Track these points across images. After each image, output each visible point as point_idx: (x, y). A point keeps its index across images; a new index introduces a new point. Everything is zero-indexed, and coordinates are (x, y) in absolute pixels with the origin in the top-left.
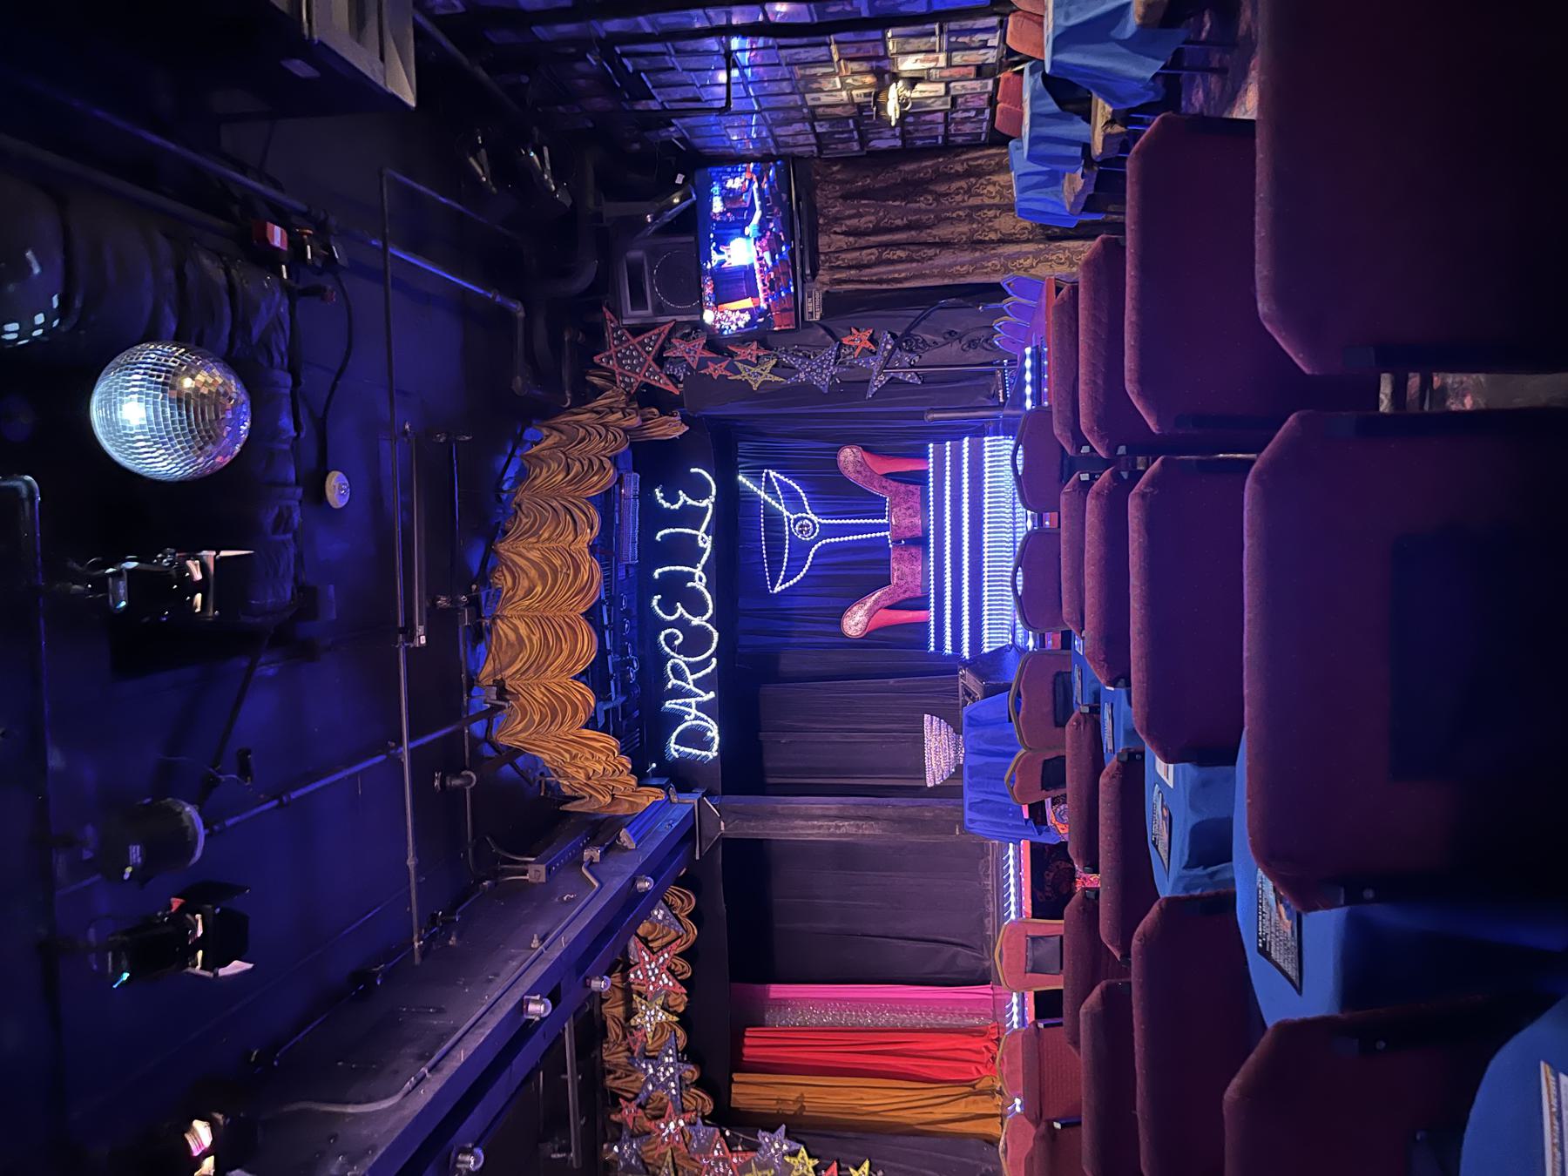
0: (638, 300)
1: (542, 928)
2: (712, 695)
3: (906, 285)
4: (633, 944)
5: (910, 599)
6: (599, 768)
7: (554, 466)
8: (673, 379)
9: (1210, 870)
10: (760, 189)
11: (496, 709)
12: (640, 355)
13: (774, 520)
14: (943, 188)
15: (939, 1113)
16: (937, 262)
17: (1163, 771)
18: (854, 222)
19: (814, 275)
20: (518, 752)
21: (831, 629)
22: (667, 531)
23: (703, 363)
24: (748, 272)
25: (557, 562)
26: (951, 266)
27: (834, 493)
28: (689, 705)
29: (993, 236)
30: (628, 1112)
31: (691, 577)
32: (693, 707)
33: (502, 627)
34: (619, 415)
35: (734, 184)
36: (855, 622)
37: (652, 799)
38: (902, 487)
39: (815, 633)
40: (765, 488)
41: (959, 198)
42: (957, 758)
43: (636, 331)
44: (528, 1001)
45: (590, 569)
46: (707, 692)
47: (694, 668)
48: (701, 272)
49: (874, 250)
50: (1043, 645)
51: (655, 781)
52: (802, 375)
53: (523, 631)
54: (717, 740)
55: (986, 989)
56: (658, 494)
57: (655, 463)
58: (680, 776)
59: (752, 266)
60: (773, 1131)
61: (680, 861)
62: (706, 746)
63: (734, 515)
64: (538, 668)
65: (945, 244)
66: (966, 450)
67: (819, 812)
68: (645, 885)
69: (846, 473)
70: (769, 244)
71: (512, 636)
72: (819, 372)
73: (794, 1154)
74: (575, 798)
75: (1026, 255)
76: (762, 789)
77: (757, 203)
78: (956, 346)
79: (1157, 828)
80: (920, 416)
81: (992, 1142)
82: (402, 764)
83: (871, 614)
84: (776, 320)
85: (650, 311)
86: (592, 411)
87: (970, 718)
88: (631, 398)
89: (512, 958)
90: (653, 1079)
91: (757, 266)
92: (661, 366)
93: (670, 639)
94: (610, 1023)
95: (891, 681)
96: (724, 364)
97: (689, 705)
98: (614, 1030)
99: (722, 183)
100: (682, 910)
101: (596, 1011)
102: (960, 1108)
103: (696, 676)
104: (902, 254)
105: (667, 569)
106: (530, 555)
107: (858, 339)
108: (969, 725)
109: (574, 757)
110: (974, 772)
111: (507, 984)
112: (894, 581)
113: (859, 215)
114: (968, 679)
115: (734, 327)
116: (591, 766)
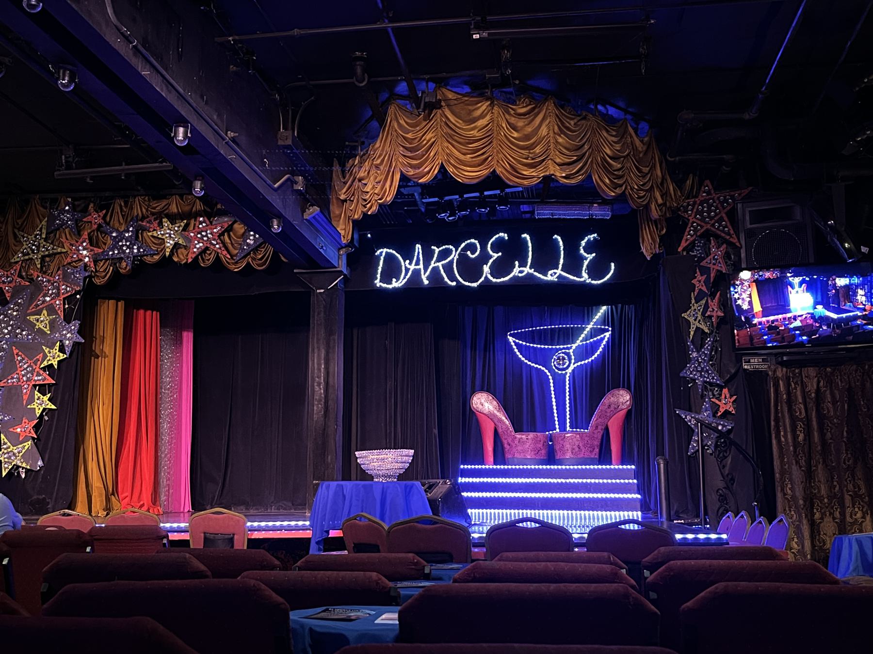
0: (757, 217)
1: (243, 140)
2: (426, 282)
3: (774, 442)
4: (226, 220)
5: (502, 446)
6: (368, 188)
7: (618, 147)
8: (691, 247)
9: (309, 649)
10: (856, 318)
11: (417, 101)
12: (711, 218)
13: (568, 336)
14: (859, 474)
15: (92, 466)
16: (794, 467)
17: (389, 618)
18: (829, 397)
19: (782, 364)
20: (382, 122)
21: (478, 382)
22: (561, 243)
23: (705, 271)
24: (784, 307)
25: (538, 150)
26: (790, 480)
27: (594, 385)
28: (417, 264)
29: (817, 516)
30: (95, 218)
31: (523, 264)
32: (416, 268)
33: (484, 106)
34: (660, 201)
35: (861, 296)
36: (484, 403)
37: (342, 232)
38: (597, 443)
39: (475, 369)
40: (594, 330)
41: (850, 487)
42: (378, 476)
43: (732, 215)
44: (186, 127)
45: (533, 176)
46: (428, 278)
47: (448, 268)
48: (784, 268)
49: (804, 414)
50: (476, 545)
51: (356, 236)
52: (695, 355)
53: (481, 123)
54: (390, 286)
55: (188, 507)
56: (591, 237)
57: (616, 240)
58: (361, 257)
59: (789, 311)
60: (79, 332)
61: (295, 254)
62: (386, 279)
63: (574, 301)
64: (451, 137)
65: (809, 475)
66: (630, 496)
67: (331, 370)
68: (276, 227)
69: (608, 395)
70: (808, 325)
71: (478, 113)
72: (698, 369)
73: (62, 350)
74: (343, 172)
75: (801, 543)
76: (350, 324)
77: (844, 315)
78: (721, 484)
79: (340, 611)
80: (660, 452)
81: (72, 506)
82: (375, 23)
83: (490, 416)
84: (743, 332)
85: (749, 226)
86: (663, 178)
87: (412, 487)
88: (675, 211)
89: (220, 116)
90: (121, 237)
91: (789, 315)
92: (702, 236)
94: (164, 203)
95: (436, 431)
96: (704, 289)
97: (417, 264)
98: (159, 205)
99: (861, 286)
100: (253, 259)
101: (174, 191)
102: (96, 483)
103: (560, 266)
104: (801, 437)
105: (530, 244)
106: (544, 126)
107: (726, 403)
108: (406, 486)
109: (377, 167)
110: (368, 490)
111: (200, 110)
112: (518, 436)
113: (834, 402)
114: (442, 487)
115: (736, 296)
116: (373, 182)
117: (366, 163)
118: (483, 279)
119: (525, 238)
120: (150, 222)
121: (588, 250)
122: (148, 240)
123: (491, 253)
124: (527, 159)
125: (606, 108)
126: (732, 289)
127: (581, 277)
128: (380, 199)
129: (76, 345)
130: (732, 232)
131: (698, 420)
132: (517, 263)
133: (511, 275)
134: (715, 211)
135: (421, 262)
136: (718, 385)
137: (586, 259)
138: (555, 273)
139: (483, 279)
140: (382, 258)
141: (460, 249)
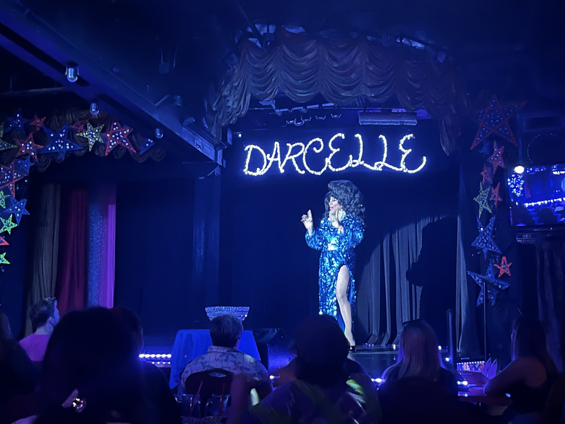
2: (282, 171)
6: (230, 104)
8: (481, 146)
25: (353, 76)
28: (276, 156)
31: (356, 157)
34: (454, 111)
46: (284, 168)
53: (309, 56)
54: (255, 174)
56: (409, 136)
62: (252, 168)
71: (308, 48)
73: (14, 220)
93: (317, 145)
97: (276, 156)
103: (384, 159)
107: (504, 268)
109: (236, 88)
117: (229, 85)
118: (325, 169)
119: (358, 138)
120: (77, 126)
121: (405, 146)
122: (77, 139)
123: (331, 148)
124: (345, 84)
125: (410, 42)
126: (509, 180)
127: (399, 167)
128: (237, 113)
129: (24, 217)
130: (512, 135)
131: (483, 280)
132: (351, 156)
133: (347, 166)
134: (499, 119)
135: (279, 156)
136: (498, 254)
137: (404, 153)
138: (380, 165)
139: (325, 169)
140: (250, 153)
141: (308, 146)
